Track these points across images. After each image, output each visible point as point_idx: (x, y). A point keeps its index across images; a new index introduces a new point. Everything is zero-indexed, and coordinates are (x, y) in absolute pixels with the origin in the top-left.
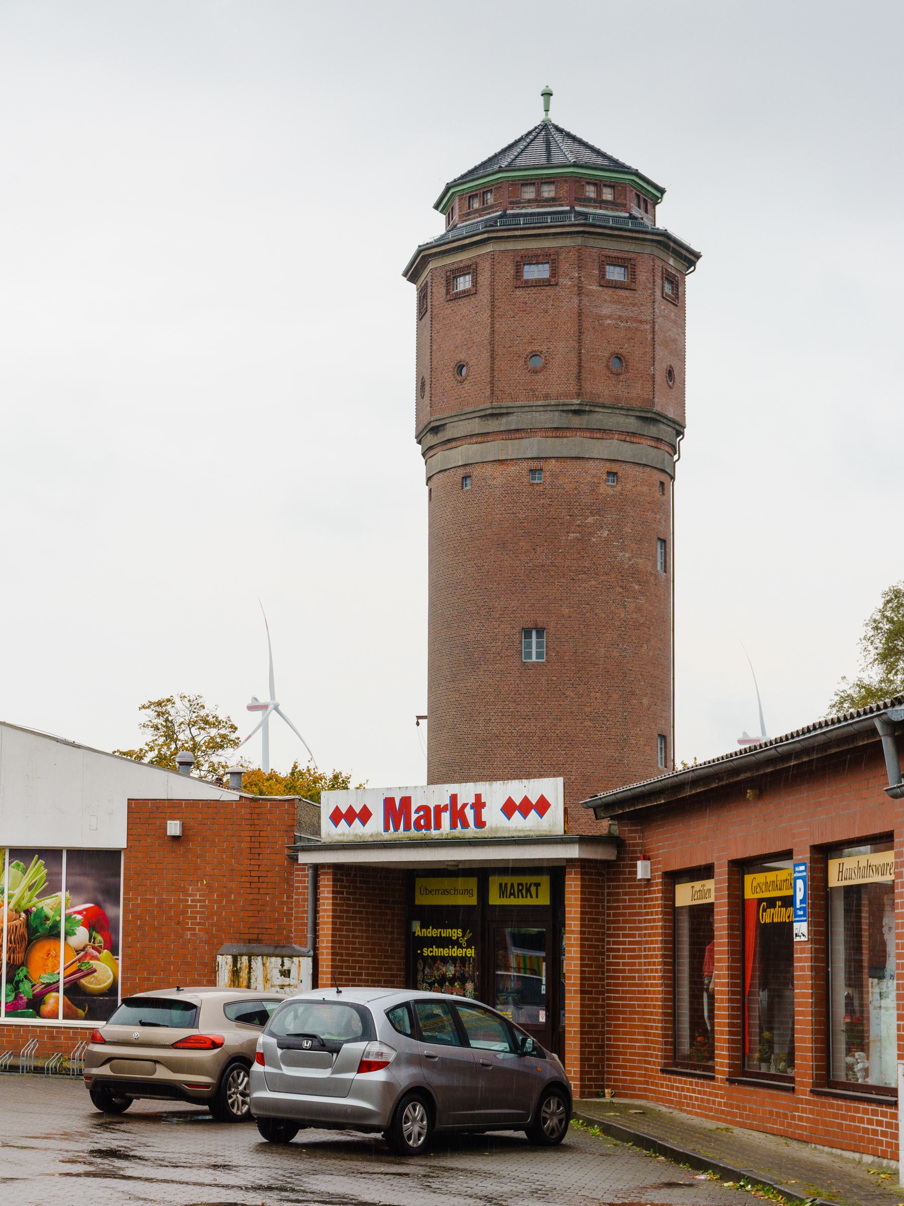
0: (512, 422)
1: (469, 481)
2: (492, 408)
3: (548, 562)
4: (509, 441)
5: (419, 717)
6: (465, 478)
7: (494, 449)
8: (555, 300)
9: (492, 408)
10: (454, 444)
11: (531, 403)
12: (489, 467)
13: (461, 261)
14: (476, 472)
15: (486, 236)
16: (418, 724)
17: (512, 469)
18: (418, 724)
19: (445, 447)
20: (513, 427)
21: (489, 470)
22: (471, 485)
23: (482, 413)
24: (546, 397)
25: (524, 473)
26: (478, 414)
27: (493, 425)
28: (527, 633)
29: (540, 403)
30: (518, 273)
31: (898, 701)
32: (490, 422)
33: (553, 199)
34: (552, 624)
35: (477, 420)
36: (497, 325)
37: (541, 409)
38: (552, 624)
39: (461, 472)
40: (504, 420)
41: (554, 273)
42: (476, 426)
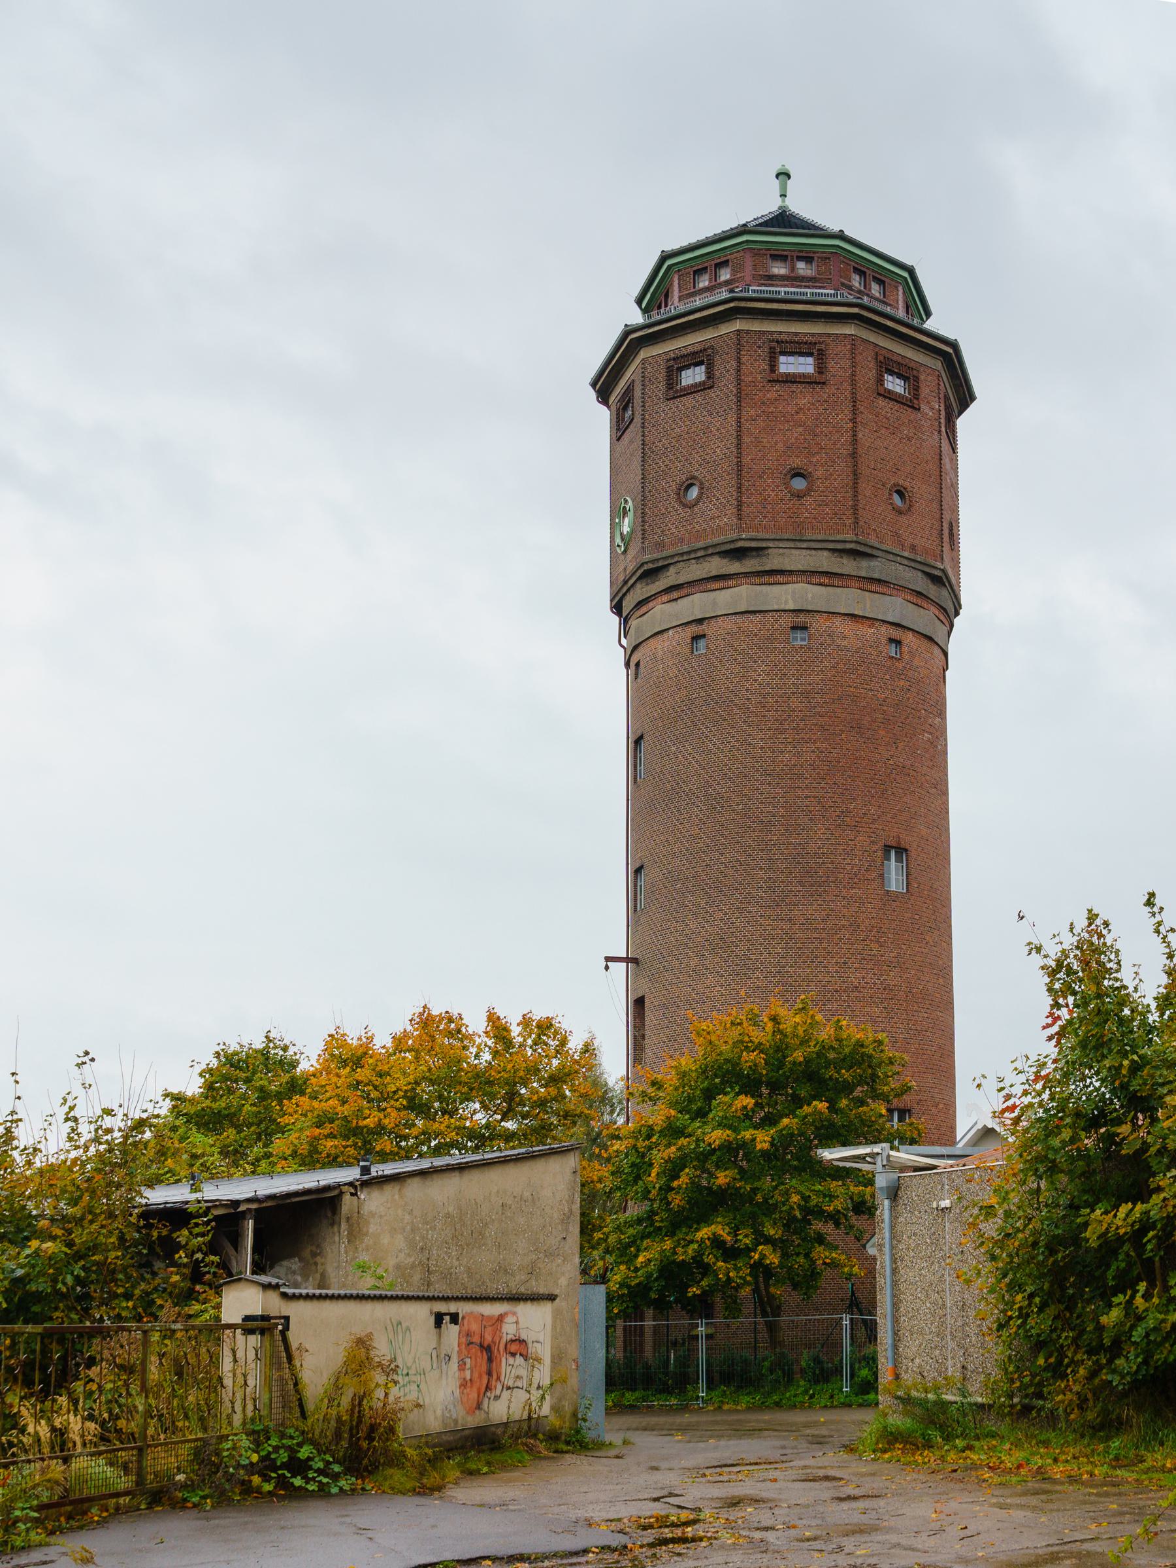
0: (864, 568)
1: (702, 643)
2: (856, 542)
3: (909, 763)
4: (867, 594)
5: (608, 959)
6: (696, 638)
7: (848, 599)
8: (787, 422)
9: (856, 542)
10: (779, 578)
11: (896, 551)
12: (838, 621)
13: (796, 334)
14: (818, 623)
15: (855, 310)
16: (607, 968)
17: (867, 630)
18: (607, 968)
19: (757, 580)
20: (876, 576)
21: (838, 624)
22: (708, 648)
23: (839, 546)
24: (913, 548)
25: (884, 640)
26: (831, 546)
27: (847, 566)
28: (887, 849)
29: (906, 554)
30: (773, 367)
31: (1171, 1065)
32: (845, 561)
33: (811, 279)
34: (915, 844)
35: (825, 553)
36: (860, 435)
37: (906, 562)
38: (915, 844)
39: (790, 619)
40: (864, 563)
41: (710, 375)
42: (824, 561)
